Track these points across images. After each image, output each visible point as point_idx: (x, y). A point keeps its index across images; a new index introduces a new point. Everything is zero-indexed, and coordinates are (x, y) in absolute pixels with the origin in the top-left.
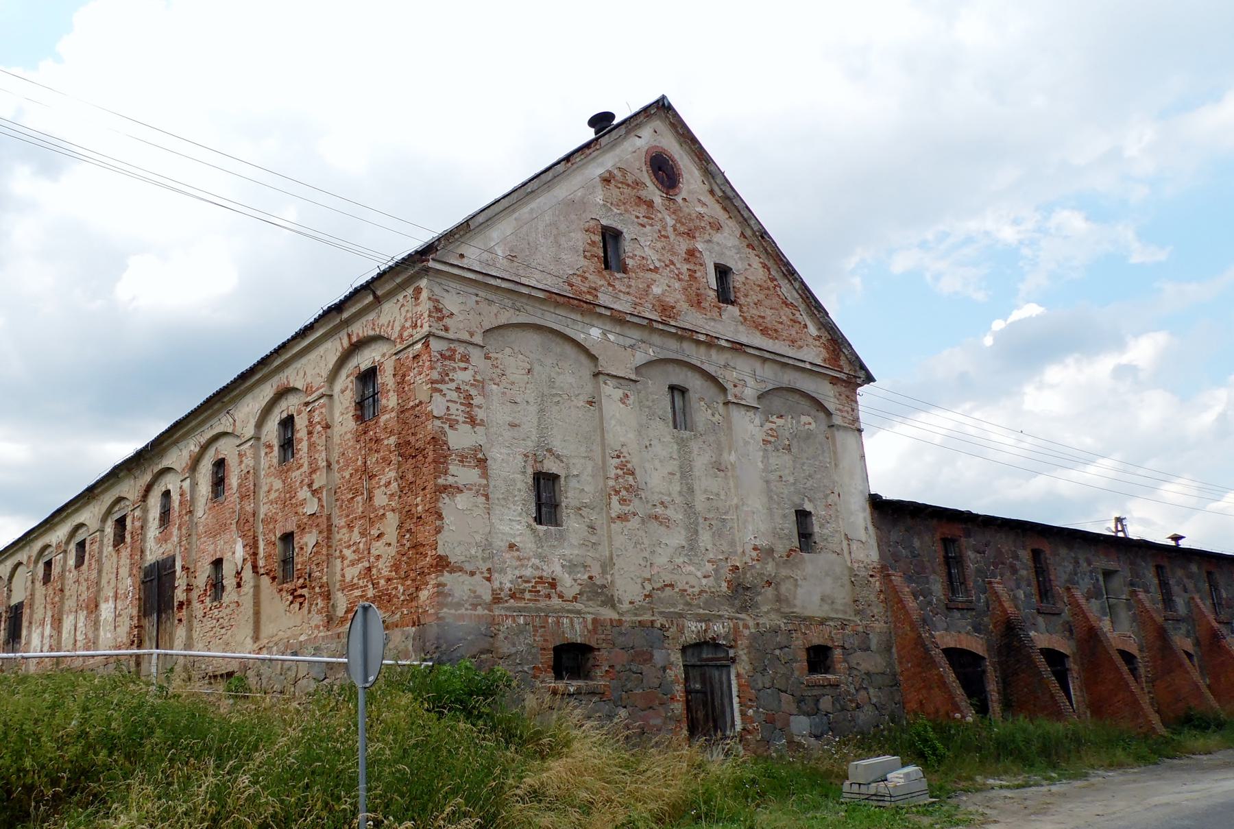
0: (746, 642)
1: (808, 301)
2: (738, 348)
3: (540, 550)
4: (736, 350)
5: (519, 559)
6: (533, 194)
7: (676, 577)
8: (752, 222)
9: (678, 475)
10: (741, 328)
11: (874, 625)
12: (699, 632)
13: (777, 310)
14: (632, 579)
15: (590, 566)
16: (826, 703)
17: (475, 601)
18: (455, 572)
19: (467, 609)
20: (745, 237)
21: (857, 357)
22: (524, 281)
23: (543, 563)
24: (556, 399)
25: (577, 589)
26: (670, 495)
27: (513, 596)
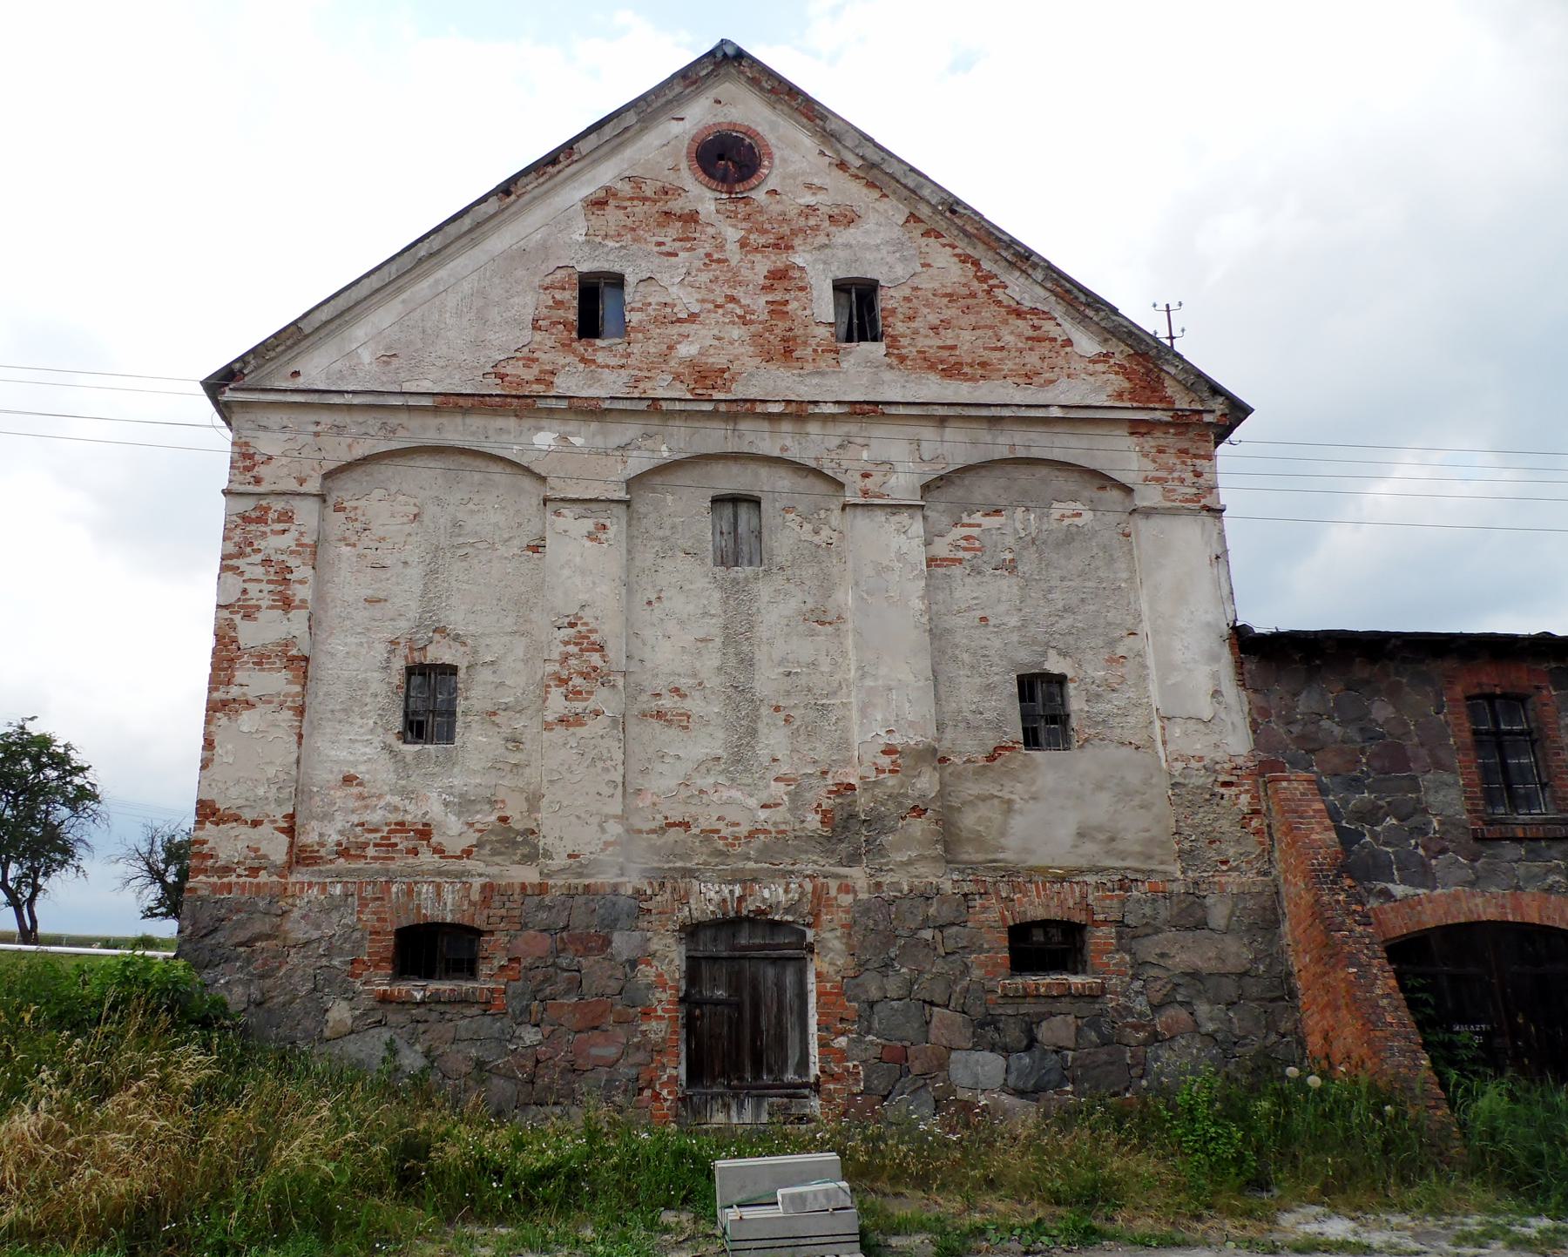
1: (1068, 297)
2: (867, 411)
3: (403, 782)
4: (863, 414)
5: (361, 797)
6: (434, 260)
7: (693, 810)
8: (926, 192)
9: (718, 641)
10: (888, 375)
11: (1223, 880)
12: (724, 900)
13: (991, 327)
14: (578, 817)
15: (503, 801)
16: (1054, 1031)
17: (256, 864)
18: (225, 822)
19: (239, 876)
20: (918, 220)
21: (1200, 375)
22: (407, 387)
23: (407, 802)
24: (461, 552)
25: (472, 838)
26: (695, 675)
27: (343, 852)
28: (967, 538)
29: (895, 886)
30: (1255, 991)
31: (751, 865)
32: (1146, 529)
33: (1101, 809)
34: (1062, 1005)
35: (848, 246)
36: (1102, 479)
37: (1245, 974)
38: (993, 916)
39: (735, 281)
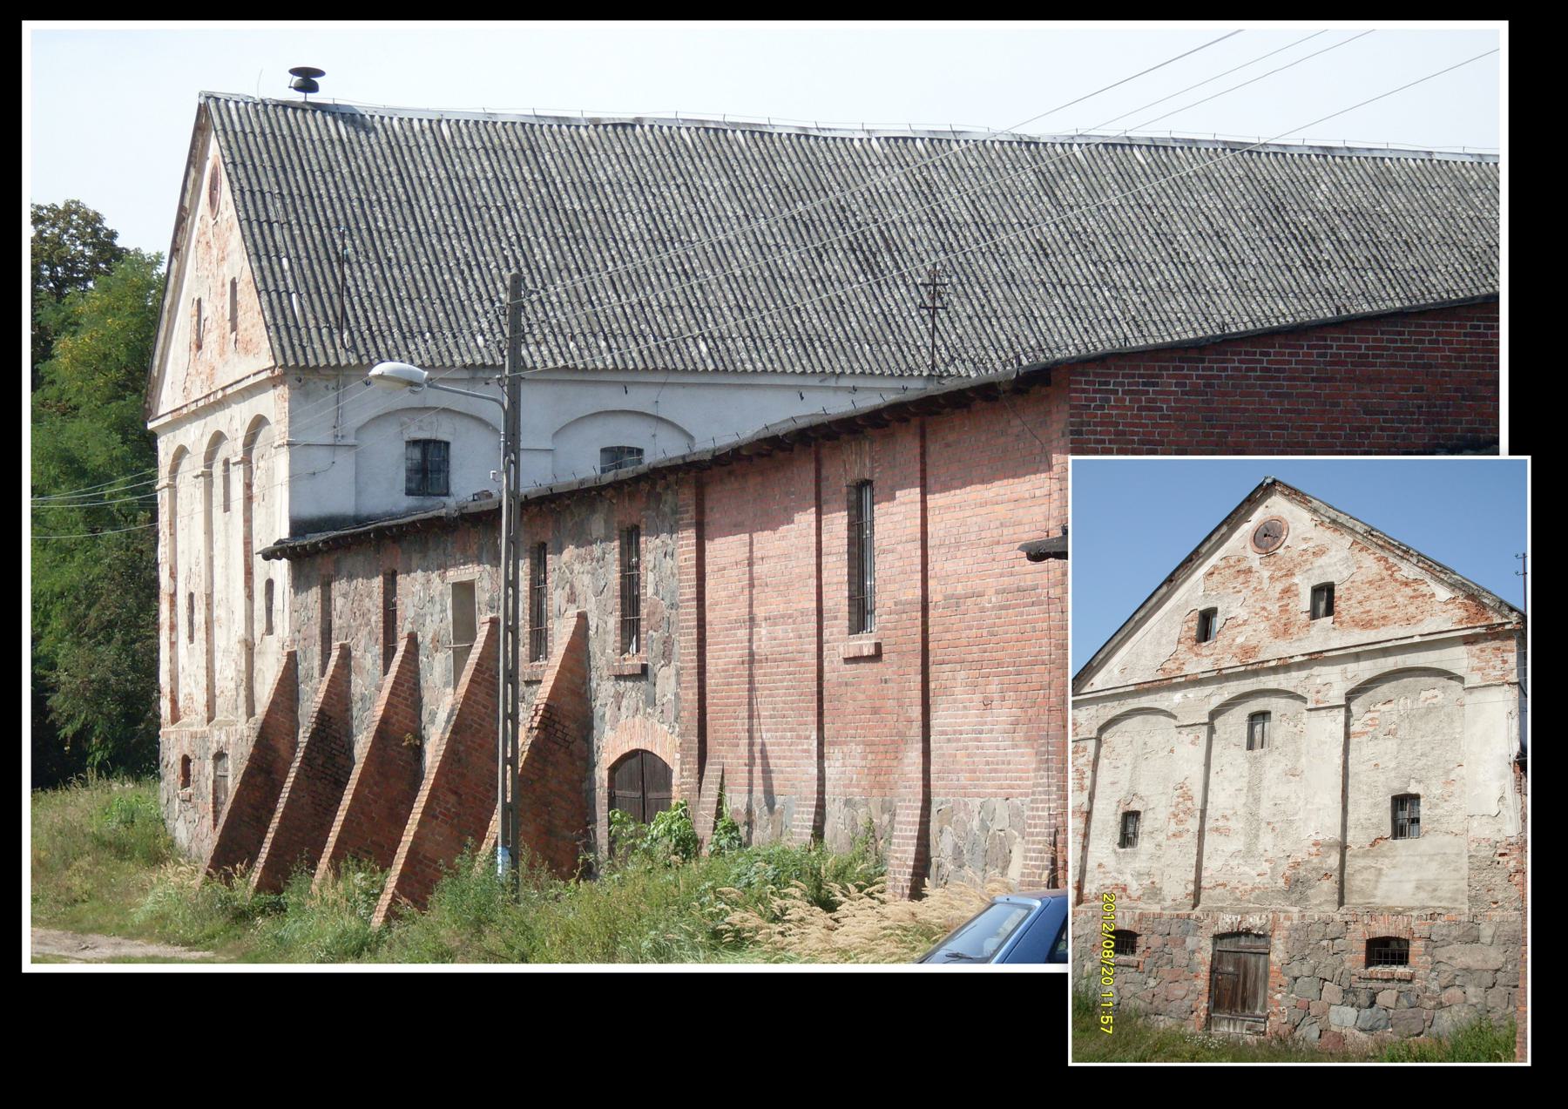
0: (1285, 933)
10: (1333, 634)
16: (1386, 997)
25: (1140, 892)
27: (1097, 898)
28: (1372, 719)
29: (1312, 917)
30: (1504, 981)
31: (1251, 905)
32: (1469, 699)
33: (1431, 871)
34: (1389, 985)
35: (1321, 566)
36: (1450, 676)
37: (1497, 970)
38: (1358, 935)
39: (1266, 599)
